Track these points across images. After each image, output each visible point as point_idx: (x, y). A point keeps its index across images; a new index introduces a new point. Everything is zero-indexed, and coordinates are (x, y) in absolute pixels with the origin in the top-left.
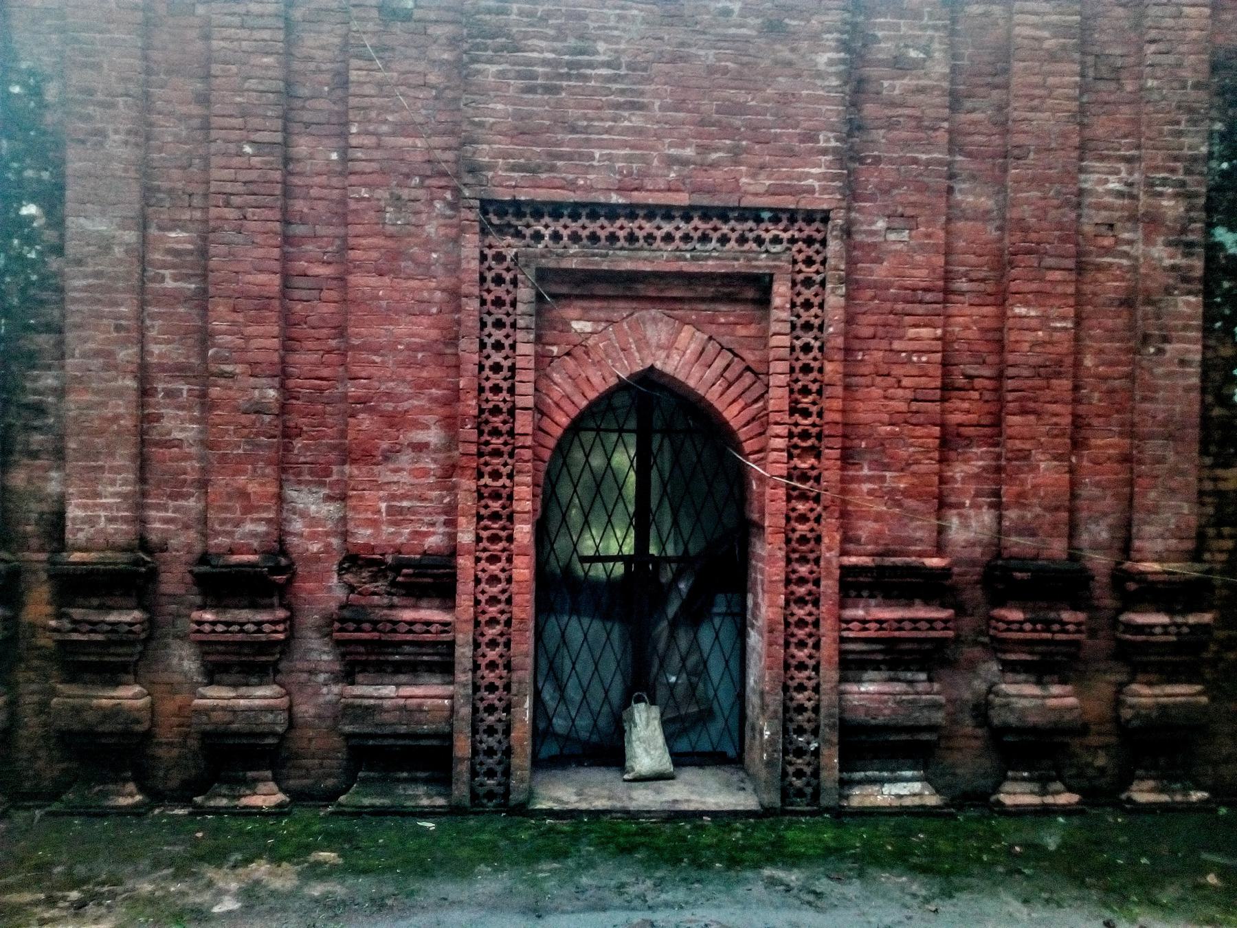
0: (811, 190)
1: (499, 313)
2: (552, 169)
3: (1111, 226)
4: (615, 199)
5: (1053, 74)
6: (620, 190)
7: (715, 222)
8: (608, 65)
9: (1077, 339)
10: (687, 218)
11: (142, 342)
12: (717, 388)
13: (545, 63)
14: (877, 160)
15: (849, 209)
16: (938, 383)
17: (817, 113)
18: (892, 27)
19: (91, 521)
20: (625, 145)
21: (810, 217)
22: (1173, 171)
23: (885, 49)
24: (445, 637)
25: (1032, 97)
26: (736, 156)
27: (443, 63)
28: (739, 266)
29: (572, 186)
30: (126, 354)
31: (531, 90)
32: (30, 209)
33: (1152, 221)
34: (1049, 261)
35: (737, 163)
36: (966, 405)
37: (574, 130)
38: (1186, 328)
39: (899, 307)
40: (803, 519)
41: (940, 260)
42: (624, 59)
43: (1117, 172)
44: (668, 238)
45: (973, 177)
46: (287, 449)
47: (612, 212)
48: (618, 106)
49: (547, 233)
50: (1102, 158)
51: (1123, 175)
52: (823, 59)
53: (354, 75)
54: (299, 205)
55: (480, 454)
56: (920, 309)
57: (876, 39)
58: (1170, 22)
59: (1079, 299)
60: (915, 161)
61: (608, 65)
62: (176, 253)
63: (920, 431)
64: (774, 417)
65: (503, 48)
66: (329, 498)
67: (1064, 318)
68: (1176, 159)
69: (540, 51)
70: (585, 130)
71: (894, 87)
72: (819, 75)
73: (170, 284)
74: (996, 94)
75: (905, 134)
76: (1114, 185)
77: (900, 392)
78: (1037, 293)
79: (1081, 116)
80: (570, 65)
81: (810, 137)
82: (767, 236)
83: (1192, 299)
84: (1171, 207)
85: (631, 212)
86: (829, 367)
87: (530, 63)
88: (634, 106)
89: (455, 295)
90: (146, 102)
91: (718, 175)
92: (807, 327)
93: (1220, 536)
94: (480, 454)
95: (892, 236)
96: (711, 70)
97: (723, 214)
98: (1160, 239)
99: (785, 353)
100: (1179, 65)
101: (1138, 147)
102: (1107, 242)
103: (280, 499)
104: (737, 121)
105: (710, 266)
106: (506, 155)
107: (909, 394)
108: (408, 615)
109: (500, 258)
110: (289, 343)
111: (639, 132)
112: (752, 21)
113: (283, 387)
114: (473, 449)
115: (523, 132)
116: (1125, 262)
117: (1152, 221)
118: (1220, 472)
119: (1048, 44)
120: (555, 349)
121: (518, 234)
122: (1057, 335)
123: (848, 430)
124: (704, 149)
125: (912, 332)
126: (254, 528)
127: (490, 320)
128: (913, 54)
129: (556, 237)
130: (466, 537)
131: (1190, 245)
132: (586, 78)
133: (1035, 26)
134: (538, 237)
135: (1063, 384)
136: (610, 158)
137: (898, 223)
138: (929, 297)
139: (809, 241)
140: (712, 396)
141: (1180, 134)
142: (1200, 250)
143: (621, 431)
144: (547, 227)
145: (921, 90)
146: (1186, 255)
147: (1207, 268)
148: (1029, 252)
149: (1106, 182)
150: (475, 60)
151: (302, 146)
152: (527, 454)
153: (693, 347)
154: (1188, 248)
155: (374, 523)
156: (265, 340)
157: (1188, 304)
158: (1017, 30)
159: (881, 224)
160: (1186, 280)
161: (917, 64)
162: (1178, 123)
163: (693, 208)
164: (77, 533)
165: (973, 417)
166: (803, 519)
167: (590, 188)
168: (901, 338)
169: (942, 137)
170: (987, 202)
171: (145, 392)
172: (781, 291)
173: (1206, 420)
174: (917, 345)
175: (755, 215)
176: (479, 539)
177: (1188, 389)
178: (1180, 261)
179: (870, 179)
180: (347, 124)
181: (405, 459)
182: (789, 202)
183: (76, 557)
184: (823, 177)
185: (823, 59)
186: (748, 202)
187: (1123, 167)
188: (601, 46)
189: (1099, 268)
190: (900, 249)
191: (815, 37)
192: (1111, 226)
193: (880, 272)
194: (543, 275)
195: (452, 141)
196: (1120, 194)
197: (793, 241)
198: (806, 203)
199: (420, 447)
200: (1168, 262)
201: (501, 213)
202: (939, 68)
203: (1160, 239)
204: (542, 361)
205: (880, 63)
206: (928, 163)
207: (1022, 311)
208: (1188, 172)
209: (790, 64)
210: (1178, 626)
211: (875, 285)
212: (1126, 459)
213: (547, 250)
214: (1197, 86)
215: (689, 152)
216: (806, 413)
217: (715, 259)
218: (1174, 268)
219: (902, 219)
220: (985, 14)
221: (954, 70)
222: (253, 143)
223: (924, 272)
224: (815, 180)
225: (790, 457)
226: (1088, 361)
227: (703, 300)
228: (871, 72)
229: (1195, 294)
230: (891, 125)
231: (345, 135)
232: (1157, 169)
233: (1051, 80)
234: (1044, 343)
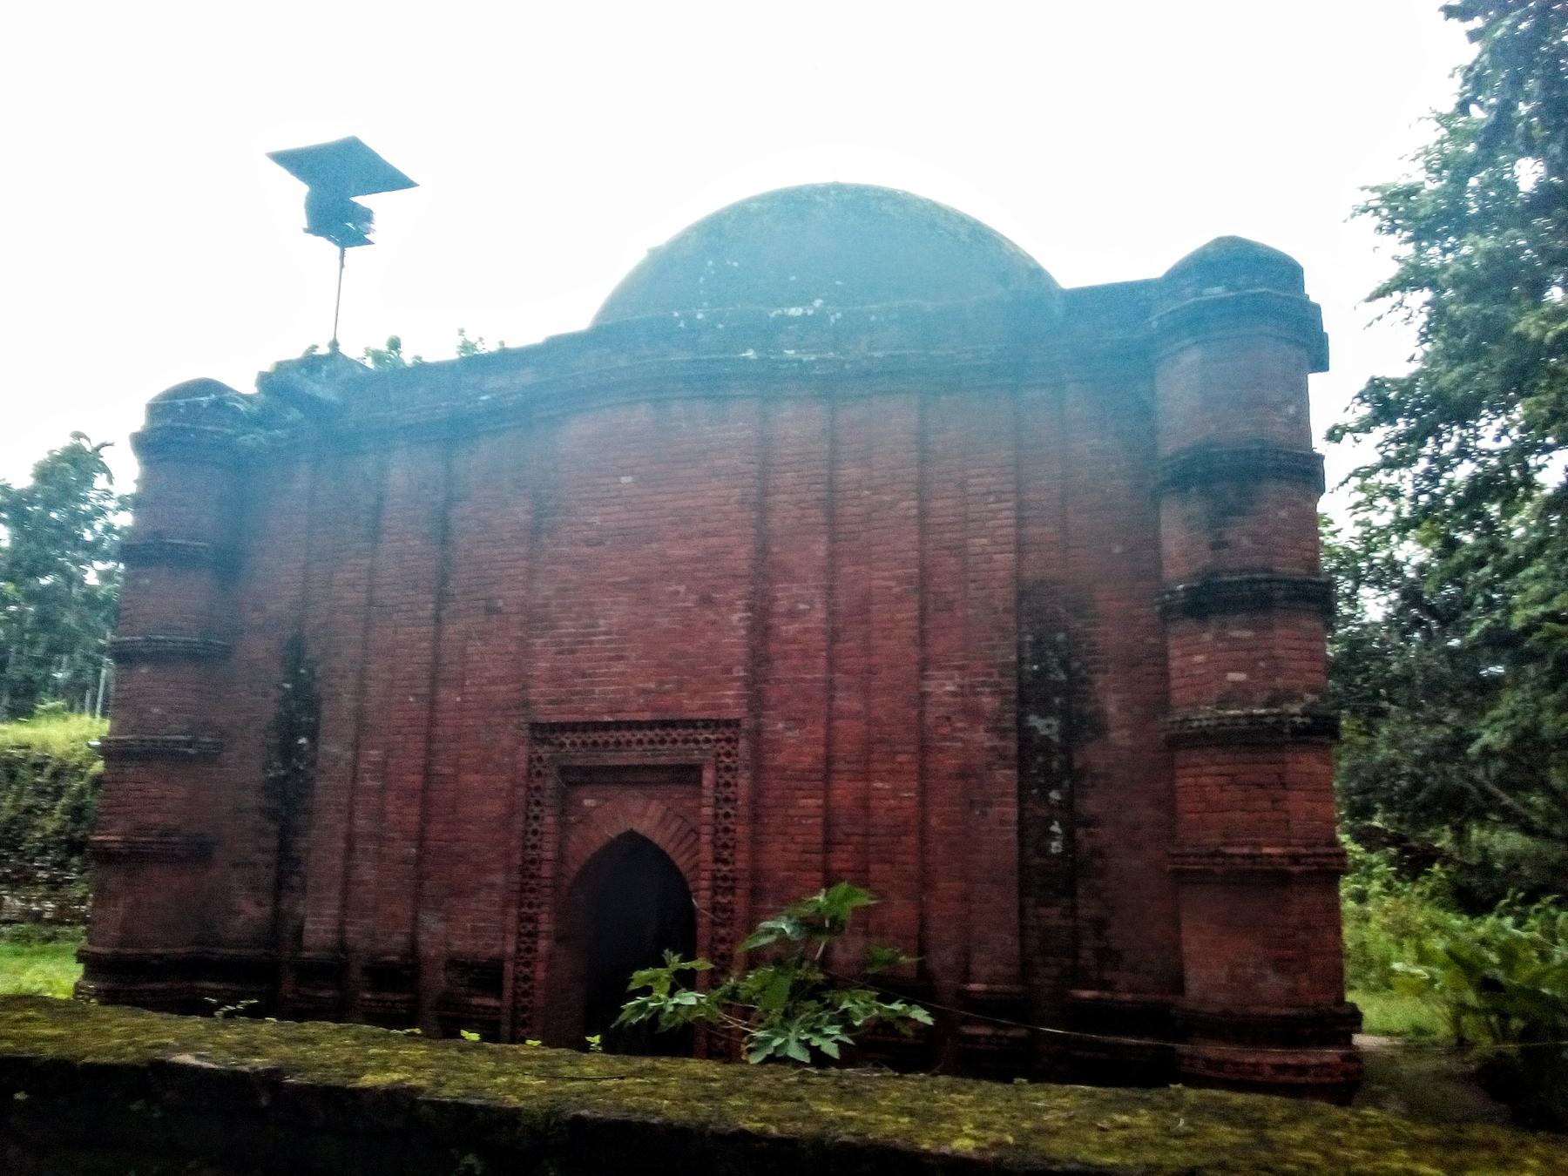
0: (727, 706)
1: (537, 796)
2: (570, 701)
3: (948, 719)
4: (607, 718)
5: (899, 611)
6: (610, 712)
7: (669, 730)
8: (605, 633)
9: (923, 804)
10: (651, 729)
11: (351, 817)
12: (672, 845)
13: (569, 635)
14: (779, 681)
15: (757, 717)
16: (820, 839)
17: (732, 654)
18: (785, 589)
19: (315, 932)
20: (614, 683)
21: (728, 724)
22: (990, 675)
23: (782, 605)
24: (495, 1018)
25: (885, 629)
26: (680, 686)
27: (517, 638)
28: (681, 760)
29: (580, 711)
30: (342, 828)
31: (561, 653)
32: (303, 741)
33: (973, 714)
34: (898, 748)
35: (680, 690)
36: (844, 856)
37: (584, 675)
38: (1004, 794)
39: (793, 784)
40: (723, 940)
41: (821, 750)
42: (615, 629)
43: (951, 678)
44: (640, 742)
45: (848, 687)
46: (420, 886)
47: (606, 726)
48: (611, 659)
49: (579, 741)
50: (940, 668)
51: (957, 680)
52: (735, 618)
53: (470, 649)
54: (439, 731)
55: (523, 891)
56: (805, 785)
57: (776, 599)
58: (985, 566)
59: (923, 772)
60: (803, 680)
61: (605, 633)
62: (374, 763)
63: (807, 876)
64: (703, 865)
65: (545, 628)
66: (442, 919)
67: (909, 790)
68: (991, 666)
69: (568, 628)
70: (590, 675)
71: (789, 629)
72: (734, 629)
73: (369, 783)
74: (863, 627)
75: (794, 662)
76: (950, 688)
77: (793, 847)
78: (889, 772)
79: (922, 639)
80: (583, 635)
81: (728, 670)
82: (701, 738)
83: (1008, 772)
84: (988, 702)
85: (618, 725)
86: (739, 829)
87: (561, 636)
88: (621, 658)
89: (514, 785)
90: (362, 674)
91: (668, 700)
92: (727, 800)
93: (1046, 965)
94: (523, 891)
95: (789, 734)
96: (667, 631)
97: (672, 724)
98: (981, 727)
99: (710, 820)
100: (992, 596)
101: (965, 658)
102: (945, 730)
103: (415, 918)
104: (681, 663)
105: (662, 760)
106: (543, 694)
107: (800, 848)
108: (476, 1001)
109: (540, 759)
110: (426, 818)
111: (622, 674)
112: (693, 597)
113: (420, 847)
114: (517, 887)
115: (557, 678)
116: (959, 744)
117: (973, 714)
118: (1042, 911)
119: (897, 590)
120: (572, 819)
121: (551, 744)
122: (906, 803)
123: (756, 875)
124: (662, 683)
125: (803, 802)
126: (399, 939)
127: (532, 800)
128: (802, 606)
129: (573, 744)
130: (511, 949)
131: (1005, 730)
132: (591, 643)
133: (884, 579)
134: (562, 745)
135: (911, 840)
136: (605, 692)
137: (791, 724)
138: (813, 776)
139: (728, 740)
140: (669, 849)
141: (993, 647)
142: (1013, 735)
143: (1400, 820)
144: (567, 738)
145: (806, 630)
146: (1003, 738)
147: (1021, 748)
148: (881, 741)
149: (943, 686)
150: (531, 637)
151: (443, 693)
152: (548, 891)
153: (659, 814)
154: (1003, 733)
155: (462, 938)
156: (412, 814)
157: (1005, 777)
158: (875, 582)
159: (780, 726)
160: (1005, 758)
161: (804, 613)
162: (991, 639)
163: (654, 722)
164: (309, 940)
165: (850, 865)
166: (723, 940)
167: (593, 712)
168: (794, 807)
169: (821, 662)
170: (857, 706)
171: (350, 849)
172: (708, 776)
173: (1023, 867)
174: (802, 812)
175: (690, 724)
176: (519, 950)
177: (1008, 842)
178: (997, 743)
179: (773, 695)
180: (464, 680)
181: (483, 894)
182: (714, 715)
183: (307, 954)
184: (735, 697)
185: (735, 618)
186: (689, 716)
187: (956, 673)
188: (602, 622)
189: (941, 750)
190: (794, 743)
191: (731, 604)
192: (948, 719)
193: (780, 759)
194: (564, 771)
195: (518, 686)
196: (954, 694)
197: (718, 740)
198: (725, 716)
199: (492, 886)
200: (988, 744)
201: (542, 732)
202: (820, 614)
203: (981, 727)
204: (564, 826)
205: (782, 615)
206: (812, 681)
207: (879, 785)
208: (1002, 675)
209: (714, 623)
210: (1000, 1038)
211: (775, 769)
212: (965, 898)
213: (575, 754)
214: (1005, 610)
215: (652, 685)
216: (725, 862)
217: (665, 757)
218: (993, 748)
219: (797, 722)
220: (856, 573)
221: (832, 613)
222: (415, 695)
223: (810, 759)
224: (731, 699)
225: (715, 893)
226: (934, 821)
227: (663, 783)
228: (775, 621)
229: (1010, 768)
230: (786, 656)
231: (463, 685)
232: (976, 675)
233: (899, 616)
234: (893, 810)
